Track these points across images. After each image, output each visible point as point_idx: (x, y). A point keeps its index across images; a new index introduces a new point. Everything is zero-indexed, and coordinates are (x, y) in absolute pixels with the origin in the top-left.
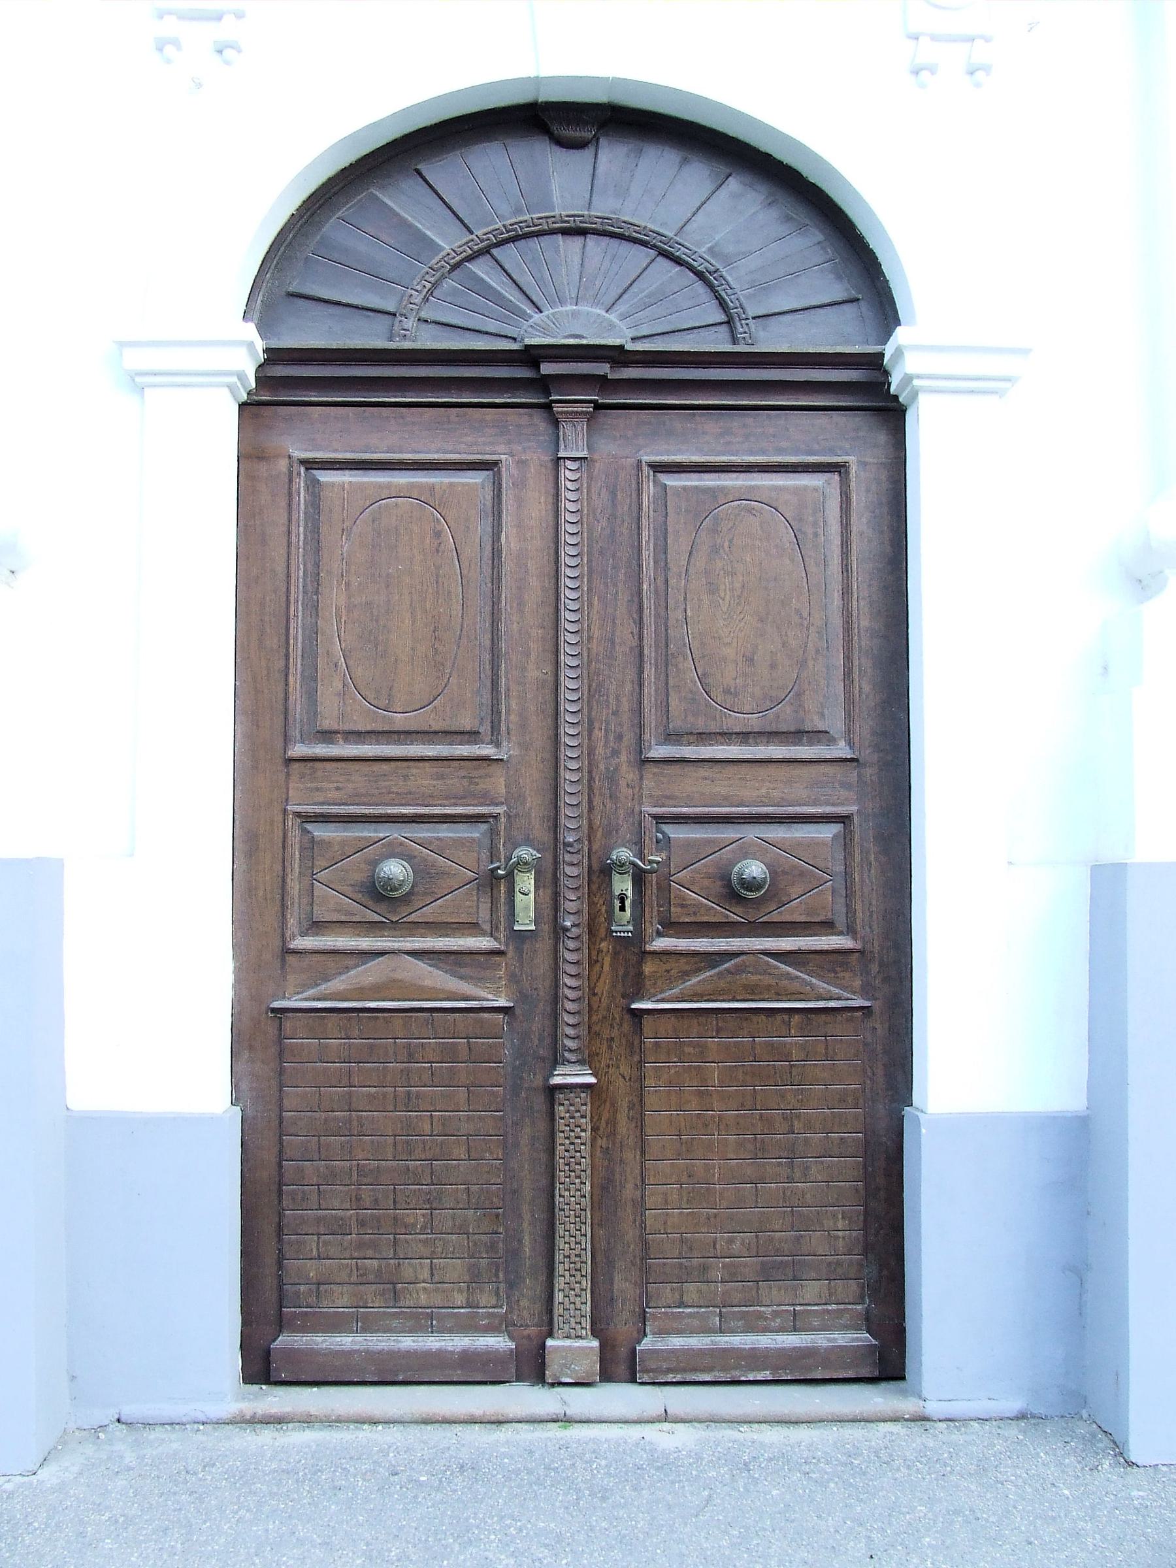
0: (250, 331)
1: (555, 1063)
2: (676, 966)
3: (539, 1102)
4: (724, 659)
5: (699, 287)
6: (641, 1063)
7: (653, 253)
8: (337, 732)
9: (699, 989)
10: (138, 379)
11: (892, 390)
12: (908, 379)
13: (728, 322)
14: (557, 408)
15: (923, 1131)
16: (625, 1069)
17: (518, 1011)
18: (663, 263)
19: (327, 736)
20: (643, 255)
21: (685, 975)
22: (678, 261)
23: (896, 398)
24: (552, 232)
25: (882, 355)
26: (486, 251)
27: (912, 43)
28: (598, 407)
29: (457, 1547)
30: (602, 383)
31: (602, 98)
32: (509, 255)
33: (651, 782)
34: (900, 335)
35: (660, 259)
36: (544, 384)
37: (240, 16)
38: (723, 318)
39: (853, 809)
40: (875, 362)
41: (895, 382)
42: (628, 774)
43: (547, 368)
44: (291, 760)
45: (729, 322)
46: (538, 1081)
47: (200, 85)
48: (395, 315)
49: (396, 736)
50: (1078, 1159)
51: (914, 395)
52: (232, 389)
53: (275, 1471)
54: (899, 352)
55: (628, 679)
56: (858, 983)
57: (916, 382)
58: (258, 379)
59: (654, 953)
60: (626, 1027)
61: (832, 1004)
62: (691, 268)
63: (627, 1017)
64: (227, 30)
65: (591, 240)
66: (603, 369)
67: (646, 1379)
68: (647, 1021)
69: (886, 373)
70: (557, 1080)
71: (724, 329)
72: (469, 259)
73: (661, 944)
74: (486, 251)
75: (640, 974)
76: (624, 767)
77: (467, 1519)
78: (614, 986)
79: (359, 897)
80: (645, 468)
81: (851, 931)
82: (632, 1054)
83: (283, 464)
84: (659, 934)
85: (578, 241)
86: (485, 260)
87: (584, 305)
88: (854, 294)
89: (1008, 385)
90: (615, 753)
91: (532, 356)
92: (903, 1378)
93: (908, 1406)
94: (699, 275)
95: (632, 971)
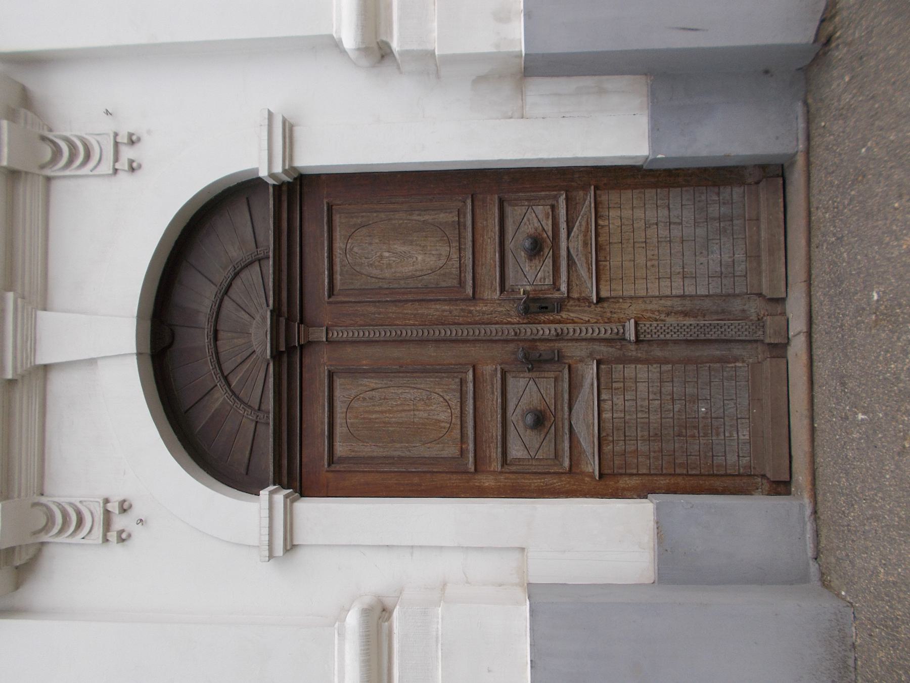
0: (264, 493)
1: (624, 339)
2: (575, 281)
3: (644, 347)
4: (424, 261)
5: (243, 275)
6: (623, 298)
7: (226, 298)
8: (462, 448)
9: (586, 270)
10: (288, 548)
11: (290, 180)
12: (285, 171)
13: (259, 260)
14: (302, 342)
15: (660, 156)
16: (626, 306)
17: (598, 357)
18: (232, 292)
19: (462, 452)
20: (227, 302)
21: (579, 277)
22: (230, 285)
23: (295, 179)
24: (216, 346)
25: (274, 186)
26: (226, 378)
27: (119, 172)
28: (302, 321)
29: (901, 385)
30: (289, 320)
31: (148, 324)
32: (228, 367)
33: (487, 295)
34: (263, 173)
35: (229, 294)
36: (290, 349)
37: (107, 501)
38: (257, 263)
39: (496, 196)
40: (278, 189)
41: (287, 179)
42: (481, 307)
43: (283, 349)
44: (476, 470)
45: (259, 260)
46: (633, 347)
47: (141, 520)
48: (257, 422)
49: (462, 240)
50: (672, 78)
51: (294, 169)
52: (293, 501)
53: (847, 480)
54: (272, 175)
55: (433, 306)
56: (581, 193)
57: (287, 167)
58: (288, 488)
59: (568, 292)
60: (605, 305)
61: (593, 205)
62: (233, 279)
63: (600, 305)
64: (113, 507)
65: (221, 327)
66: (283, 320)
67: (783, 289)
68: (604, 294)
69: (283, 183)
70: (633, 338)
71: (263, 263)
72: (229, 385)
73: (564, 288)
74: (226, 378)
75: (578, 299)
76: (478, 308)
77: (879, 380)
78: (585, 312)
79: (543, 436)
80: (331, 300)
81: (556, 198)
82: (618, 302)
83: (330, 475)
84: (559, 290)
85: (221, 335)
86: (230, 378)
87: (252, 330)
88: (245, 200)
89: (287, 124)
90: (470, 312)
91: (277, 356)
92: (782, 165)
93: (800, 161)
94: (237, 274)
95: (577, 303)
